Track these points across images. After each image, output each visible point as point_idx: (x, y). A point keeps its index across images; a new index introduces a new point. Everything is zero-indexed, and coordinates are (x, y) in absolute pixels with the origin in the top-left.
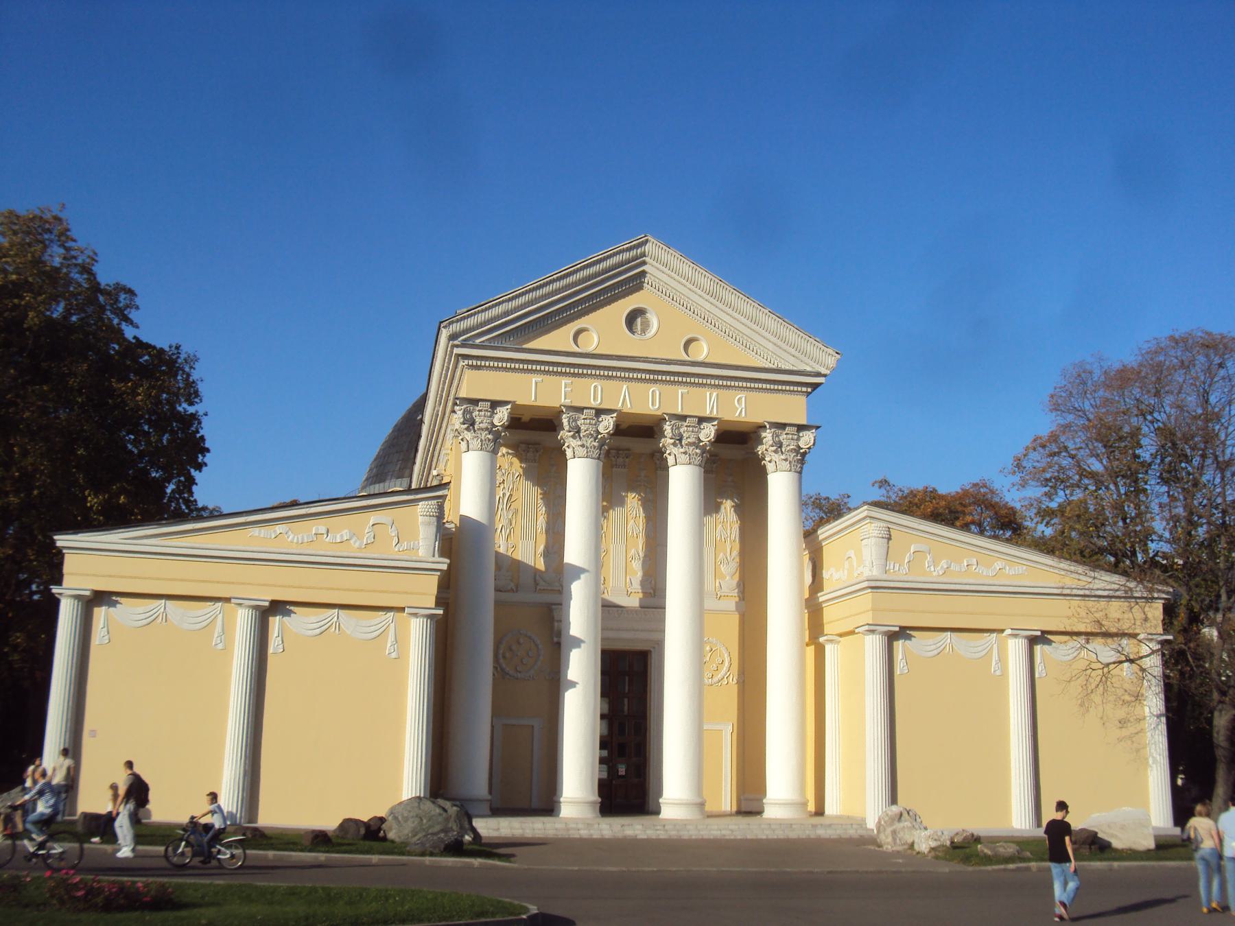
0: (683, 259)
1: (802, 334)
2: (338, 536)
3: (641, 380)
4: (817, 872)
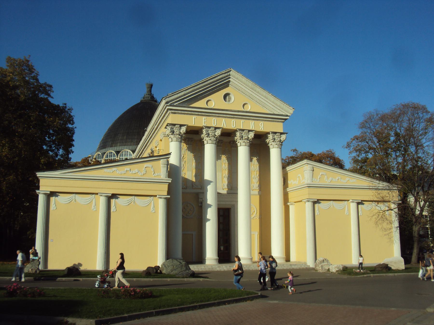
0: (243, 77)
1: (282, 102)
2: (134, 171)
3: (229, 117)
4: (307, 279)
